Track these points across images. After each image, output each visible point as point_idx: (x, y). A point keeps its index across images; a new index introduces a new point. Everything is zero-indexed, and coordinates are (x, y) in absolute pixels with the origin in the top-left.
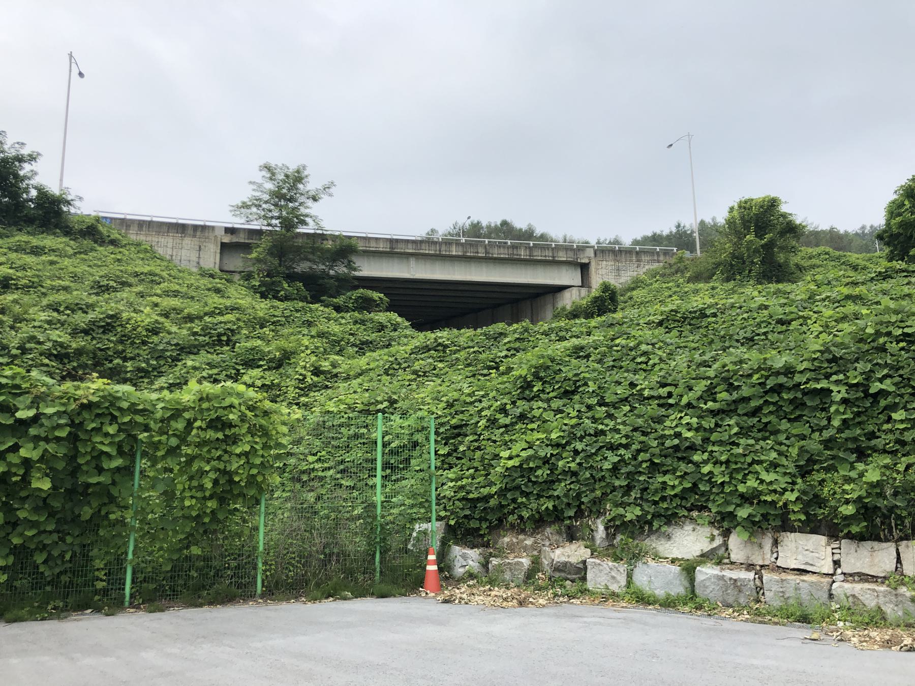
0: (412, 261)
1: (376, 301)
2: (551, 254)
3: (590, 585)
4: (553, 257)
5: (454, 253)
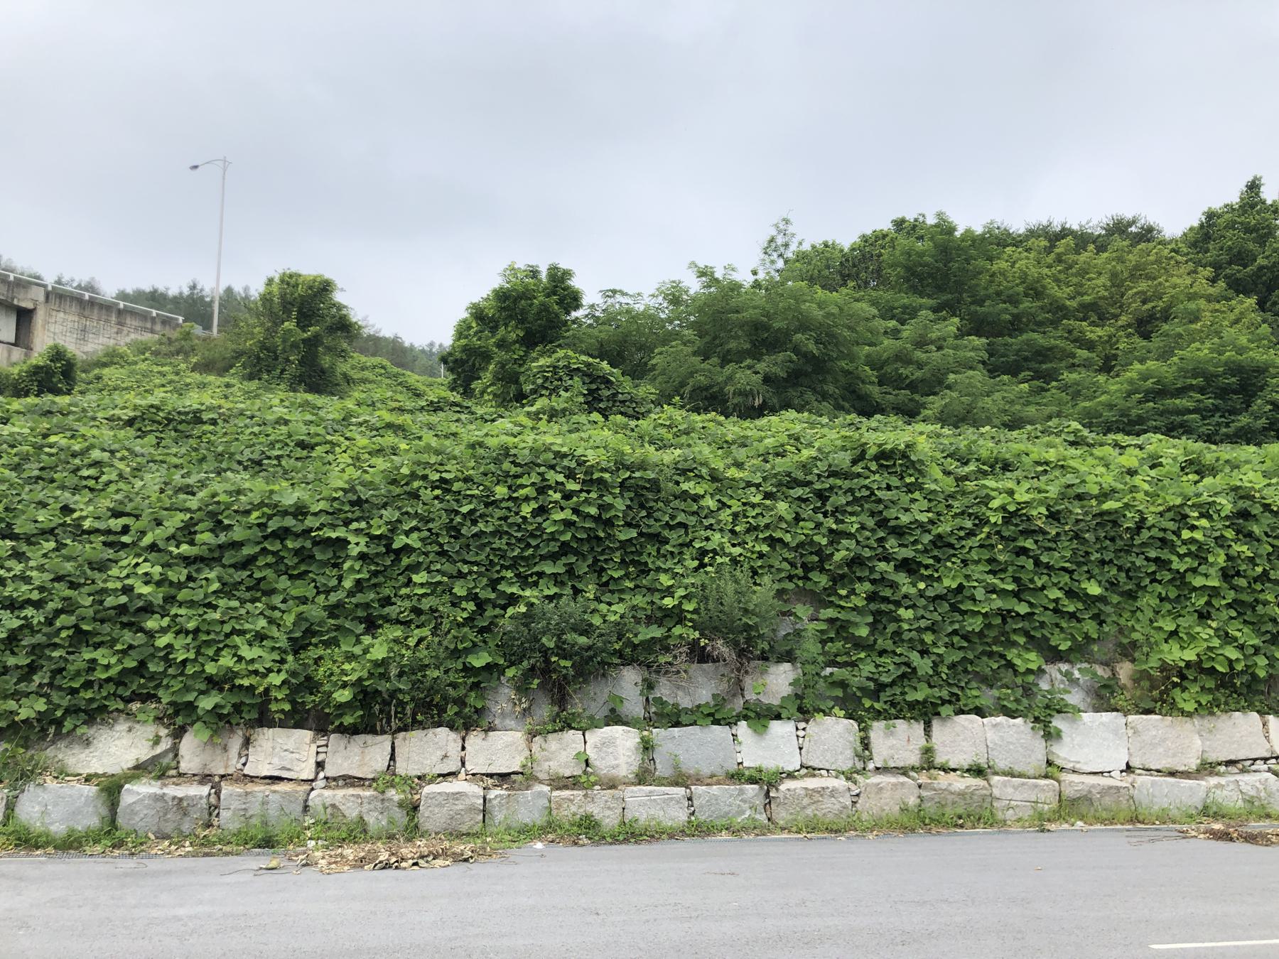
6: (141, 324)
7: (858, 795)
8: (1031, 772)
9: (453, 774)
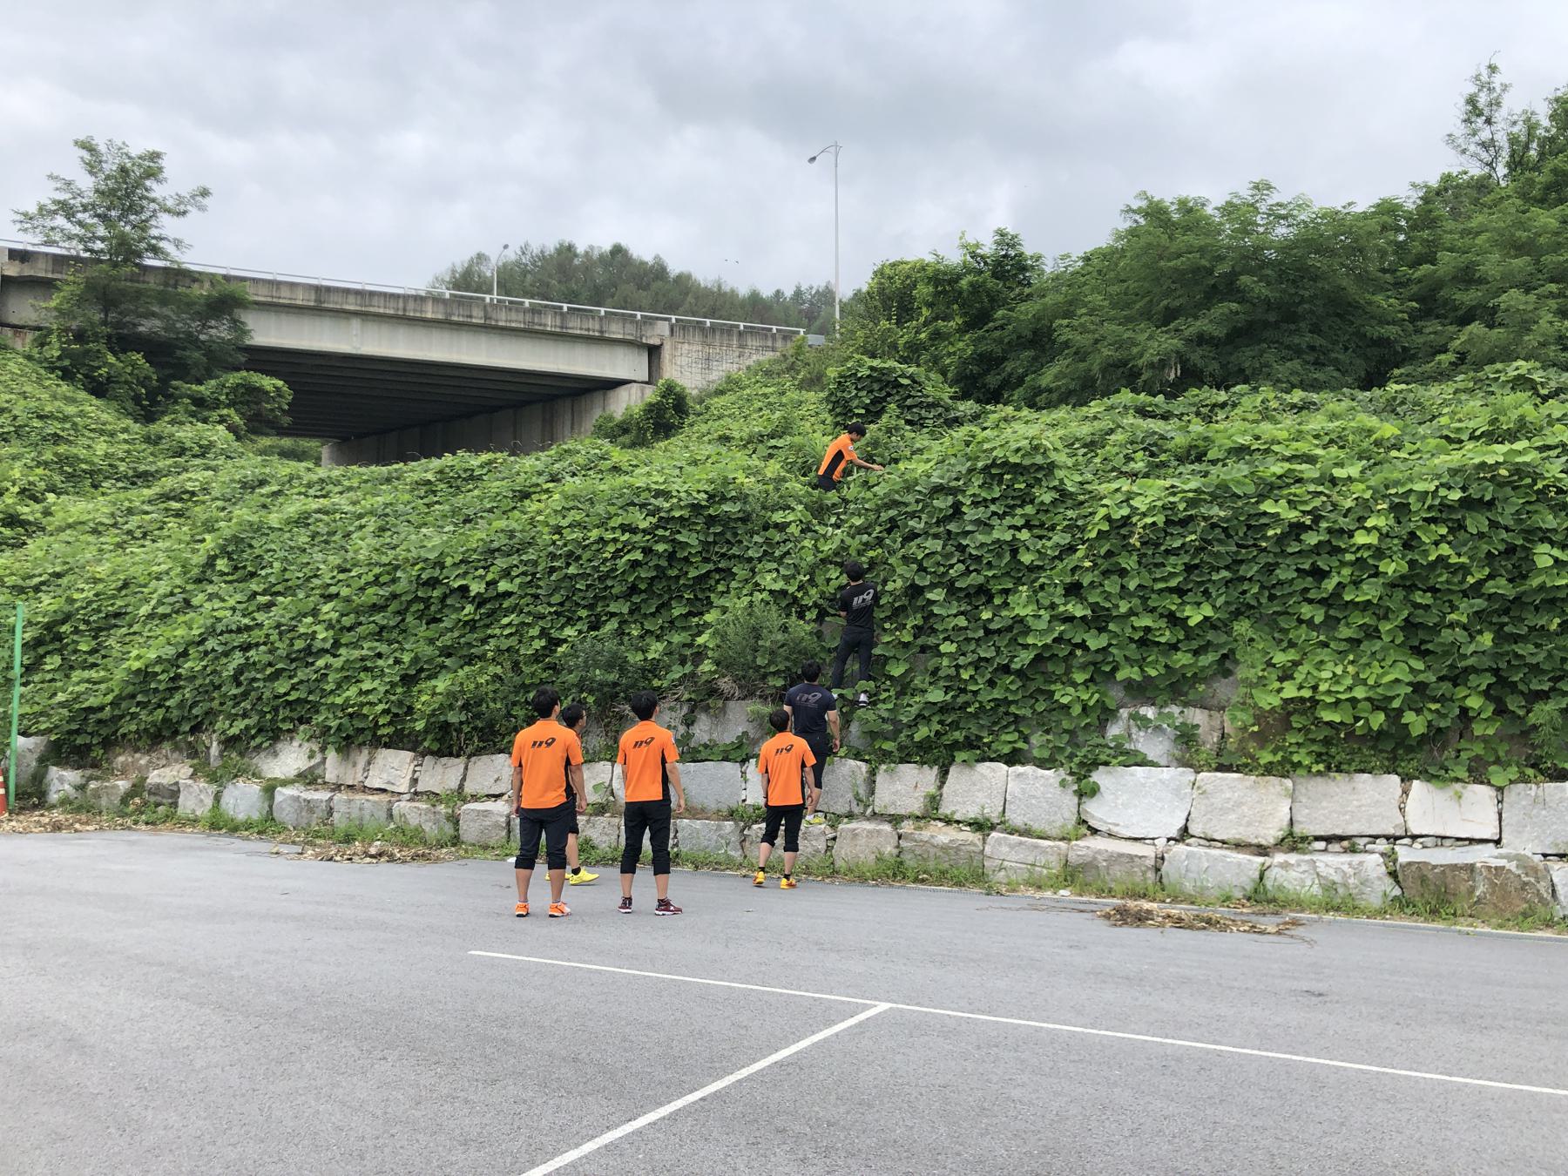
0: (356, 323)
1: (267, 393)
2: (597, 327)
3: (180, 811)
5: (429, 315)
7: (834, 839)
8: (1054, 833)
9: (498, 796)
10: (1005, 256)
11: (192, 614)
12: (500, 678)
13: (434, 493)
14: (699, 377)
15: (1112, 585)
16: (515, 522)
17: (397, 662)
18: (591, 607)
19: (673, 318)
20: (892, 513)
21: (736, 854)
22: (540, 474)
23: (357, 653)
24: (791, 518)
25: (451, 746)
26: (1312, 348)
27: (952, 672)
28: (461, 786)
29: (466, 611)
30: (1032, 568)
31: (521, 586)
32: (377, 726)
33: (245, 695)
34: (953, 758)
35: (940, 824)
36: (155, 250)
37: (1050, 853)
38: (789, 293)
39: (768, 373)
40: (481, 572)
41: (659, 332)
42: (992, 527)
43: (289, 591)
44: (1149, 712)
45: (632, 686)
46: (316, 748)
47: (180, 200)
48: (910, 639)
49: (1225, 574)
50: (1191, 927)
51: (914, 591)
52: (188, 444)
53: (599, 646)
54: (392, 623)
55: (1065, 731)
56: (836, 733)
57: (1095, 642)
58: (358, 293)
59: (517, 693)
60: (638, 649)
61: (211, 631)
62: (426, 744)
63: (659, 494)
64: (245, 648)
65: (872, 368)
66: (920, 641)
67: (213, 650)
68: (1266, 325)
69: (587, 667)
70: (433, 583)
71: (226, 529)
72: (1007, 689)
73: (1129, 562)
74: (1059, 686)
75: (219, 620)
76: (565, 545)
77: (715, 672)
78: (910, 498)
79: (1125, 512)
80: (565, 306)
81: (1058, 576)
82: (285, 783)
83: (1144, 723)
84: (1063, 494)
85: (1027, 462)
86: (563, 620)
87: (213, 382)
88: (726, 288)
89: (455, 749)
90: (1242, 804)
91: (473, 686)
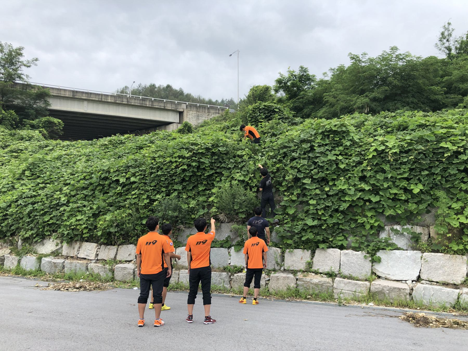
0: (85, 103)
1: (56, 124)
2: (163, 105)
3: (4, 267)
4: (164, 107)
5: (109, 101)
6: (215, 111)
7: (269, 280)
10: (303, 75)
11: (15, 191)
12: (131, 215)
13: (108, 148)
14: (195, 122)
15: (380, 176)
16: (138, 156)
17: (91, 208)
18: (167, 187)
19: (187, 103)
20: (285, 150)
21: (228, 286)
22: (147, 141)
23: (75, 205)
24: (244, 153)
25: (111, 242)
26: (412, 102)
27: (315, 211)
28: (115, 257)
29: (118, 189)
30: (345, 170)
31: (139, 179)
32: (83, 233)
33: (32, 221)
34: (318, 247)
35: (313, 274)
36: (20, 77)
37: (362, 287)
38: (220, 101)
39: (217, 120)
40: (124, 174)
41: (183, 107)
42: (327, 155)
43: (52, 182)
44: (398, 227)
45: (184, 217)
46: (59, 242)
47: (28, 62)
48: (296, 199)
49: (426, 172)
50: (451, 327)
51: (297, 180)
52: (24, 136)
53: (170, 202)
54: (90, 194)
55: (364, 236)
56: (269, 236)
57: (375, 199)
58: (86, 93)
59: (137, 221)
60: (185, 203)
61: (21, 197)
62: (102, 240)
63: (193, 144)
64: (33, 203)
65: (265, 106)
66: (300, 199)
67: (21, 204)
68: (396, 95)
69: (166, 210)
70: (106, 179)
71: (30, 160)
72: (338, 218)
73: (387, 168)
74: (359, 217)
75: (24, 193)
76: (157, 164)
77: (217, 212)
78: (292, 145)
79: (383, 147)
80: (153, 99)
81: (357, 172)
82: (46, 256)
83: (397, 232)
84: (354, 143)
85: (339, 130)
86: (156, 192)
87: (37, 120)
88: (202, 98)
89: (113, 243)
90: (445, 266)
91: (120, 218)
